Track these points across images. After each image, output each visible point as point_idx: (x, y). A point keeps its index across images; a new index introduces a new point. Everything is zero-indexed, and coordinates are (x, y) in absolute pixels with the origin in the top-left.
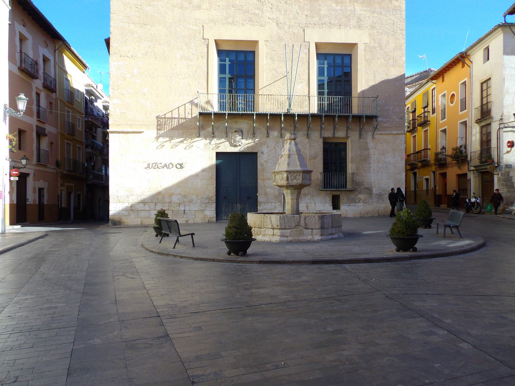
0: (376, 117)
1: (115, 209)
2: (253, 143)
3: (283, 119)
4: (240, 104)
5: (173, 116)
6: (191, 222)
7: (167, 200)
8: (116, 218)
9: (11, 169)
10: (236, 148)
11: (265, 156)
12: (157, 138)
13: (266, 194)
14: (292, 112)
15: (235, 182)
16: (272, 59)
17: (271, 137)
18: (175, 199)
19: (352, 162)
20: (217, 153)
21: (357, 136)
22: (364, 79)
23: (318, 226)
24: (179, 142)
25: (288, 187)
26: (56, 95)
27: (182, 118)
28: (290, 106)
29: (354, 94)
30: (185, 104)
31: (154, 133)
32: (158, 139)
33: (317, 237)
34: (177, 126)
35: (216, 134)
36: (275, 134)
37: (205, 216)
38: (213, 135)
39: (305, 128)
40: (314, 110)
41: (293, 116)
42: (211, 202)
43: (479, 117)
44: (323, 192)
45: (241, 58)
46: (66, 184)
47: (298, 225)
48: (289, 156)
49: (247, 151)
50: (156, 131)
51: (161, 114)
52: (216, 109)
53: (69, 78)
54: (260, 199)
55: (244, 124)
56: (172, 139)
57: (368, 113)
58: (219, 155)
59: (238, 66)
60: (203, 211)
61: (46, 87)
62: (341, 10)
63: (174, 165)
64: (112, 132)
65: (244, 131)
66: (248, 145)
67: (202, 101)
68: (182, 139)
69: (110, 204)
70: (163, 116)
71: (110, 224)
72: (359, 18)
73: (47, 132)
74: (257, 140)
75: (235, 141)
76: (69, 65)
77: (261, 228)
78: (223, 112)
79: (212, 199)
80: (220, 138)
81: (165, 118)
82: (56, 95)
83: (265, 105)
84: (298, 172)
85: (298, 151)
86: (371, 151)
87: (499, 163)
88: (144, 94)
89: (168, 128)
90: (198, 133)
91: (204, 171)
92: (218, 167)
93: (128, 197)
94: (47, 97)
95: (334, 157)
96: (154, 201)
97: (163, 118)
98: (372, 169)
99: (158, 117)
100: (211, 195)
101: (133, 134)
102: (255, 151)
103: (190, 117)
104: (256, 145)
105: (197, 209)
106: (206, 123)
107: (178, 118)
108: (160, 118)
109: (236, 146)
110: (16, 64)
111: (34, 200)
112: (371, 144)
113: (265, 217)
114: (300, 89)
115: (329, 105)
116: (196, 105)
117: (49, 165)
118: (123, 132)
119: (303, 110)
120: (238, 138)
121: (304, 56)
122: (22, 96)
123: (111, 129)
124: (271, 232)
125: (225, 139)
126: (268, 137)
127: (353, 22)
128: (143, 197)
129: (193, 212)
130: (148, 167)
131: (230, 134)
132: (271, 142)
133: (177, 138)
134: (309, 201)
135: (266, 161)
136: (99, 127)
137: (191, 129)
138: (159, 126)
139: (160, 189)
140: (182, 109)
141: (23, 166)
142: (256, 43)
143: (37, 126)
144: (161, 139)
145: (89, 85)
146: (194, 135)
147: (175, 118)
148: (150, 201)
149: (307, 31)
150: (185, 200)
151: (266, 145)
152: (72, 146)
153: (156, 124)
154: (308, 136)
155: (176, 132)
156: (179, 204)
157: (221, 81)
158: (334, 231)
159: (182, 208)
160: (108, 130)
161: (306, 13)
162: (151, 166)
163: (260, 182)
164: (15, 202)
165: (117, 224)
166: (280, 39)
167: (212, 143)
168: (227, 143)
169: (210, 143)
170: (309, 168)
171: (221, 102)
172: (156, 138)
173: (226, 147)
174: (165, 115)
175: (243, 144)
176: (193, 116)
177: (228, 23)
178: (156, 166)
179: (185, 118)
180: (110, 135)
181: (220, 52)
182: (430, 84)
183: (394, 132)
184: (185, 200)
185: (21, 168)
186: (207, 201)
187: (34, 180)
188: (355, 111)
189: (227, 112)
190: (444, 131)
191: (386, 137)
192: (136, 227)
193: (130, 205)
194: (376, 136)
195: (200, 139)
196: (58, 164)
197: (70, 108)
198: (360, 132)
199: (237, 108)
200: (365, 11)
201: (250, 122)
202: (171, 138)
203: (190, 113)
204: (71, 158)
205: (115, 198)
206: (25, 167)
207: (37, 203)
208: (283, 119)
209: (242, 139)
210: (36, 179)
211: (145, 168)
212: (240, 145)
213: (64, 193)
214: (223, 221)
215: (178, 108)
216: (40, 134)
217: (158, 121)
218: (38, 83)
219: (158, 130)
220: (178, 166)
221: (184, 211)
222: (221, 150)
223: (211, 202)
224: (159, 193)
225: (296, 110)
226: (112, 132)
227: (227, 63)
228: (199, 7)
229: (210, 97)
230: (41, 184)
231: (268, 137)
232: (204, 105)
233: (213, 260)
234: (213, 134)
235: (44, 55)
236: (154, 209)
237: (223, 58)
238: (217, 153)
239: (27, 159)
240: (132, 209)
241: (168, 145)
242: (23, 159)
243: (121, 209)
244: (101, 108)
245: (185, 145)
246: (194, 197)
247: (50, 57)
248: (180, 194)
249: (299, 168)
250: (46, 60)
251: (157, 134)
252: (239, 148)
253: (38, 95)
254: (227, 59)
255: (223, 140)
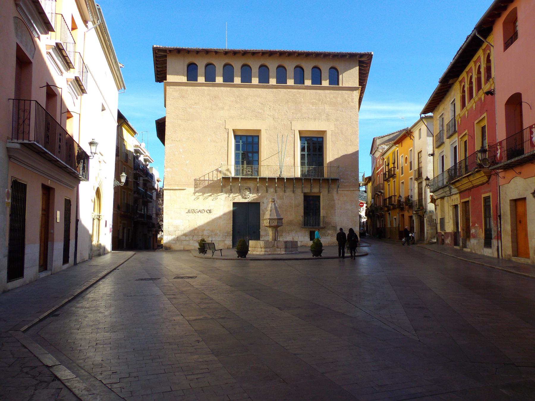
0: (338, 179)
7: (200, 234)
8: (167, 245)
11: (265, 205)
12: (195, 193)
14: (282, 176)
15: (245, 221)
16: (270, 141)
17: (269, 192)
19: (323, 209)
20: (234, 203)
21: (327, 192)
22: (331, 154)
23: (284, 247)
25: (270, 227)
29: (325, 165)
31: (192, 190)
33: (284, 253)
35: (233, 190)
36: (272, 190)
37: (225, 244)
38: (231, 191)
40: (298, 175)
41: (283, 179)
43: (417, 177)
44: (304, 229)
45: (250, 140)
46: (123, 222)
47: (274, 246)
48: (271, 211)
51: (197, 178)
52: (233, 175)
55: (251, 184)
57: (333, 177)
58: (235, 204)
59: (248, 146)
60: (224, 241)
62: (316, 109)
67: (223, 169)
72: (328, 115)
75: (245, 195)
80: (235, 193)
81: (200, 180)
83: (265, 172)
84: (274, 219)
85: (276, 208)
86: (336, 202)
87: (426, 209)
89: (202, 186)
91: (224, 214)
92: (234, 212)
95: (311, 206)
98: (337, 214)
104: (259, 197)
106: (226, 184)
107: (209, 180)
109: (246, 198)
112: (336, 197)
114: (288, 160)
115: (308, 171)
116: (220, 172)
118: (173, 190)
121: (291, 138)
122: (124, 174)
124: (260, 250)
126: (267, 192)
127: (324, 117)
128: (185, 232)
130: (189, 212)
131: (242, 190)
136: (142, 176)
138: (196, 186)
139: (196, 226)
140: (211, 174)
142: (259, 131)
144: (197, 194)
145: (137, 146)
149: (293, 123)
154: (294, 192)
157: (237, 155)
158: (293, 249)
161: (292, 111)
165: (167, 249)
166: (275, 128)
168: (240, 197)
170: (282, 217)
173: (239, 199)
175: (250, 197)
177: (241, 119)
178: (193, 211)
181: (236, 136)
182: (394, 147)
183: (351, 189)
186: (226, 234)
188: (326, 176)
190: (403, 183)
191: (345, 192)
192: (180, 251)
194: (339, 192)
198: (329, 189)
200: (332, 109)
202: (204, 193)
213: (121, 228)
220: (208, 212)
222: (236, 201)
224: (195, 229)
225: (286, 175)
227: (241, 143)
228: (223, 109)
229: (229, 167)
231: (267, 192)
232: (225, 172)
233: (231, 259)
237: (238, 140)
238: (234, 203)
240: (177, 239)
244: (143, 161)
245: (213, 198)
246: (218, 232)
249: (276, 217)
254: (241, 141)
255: (237, 194)
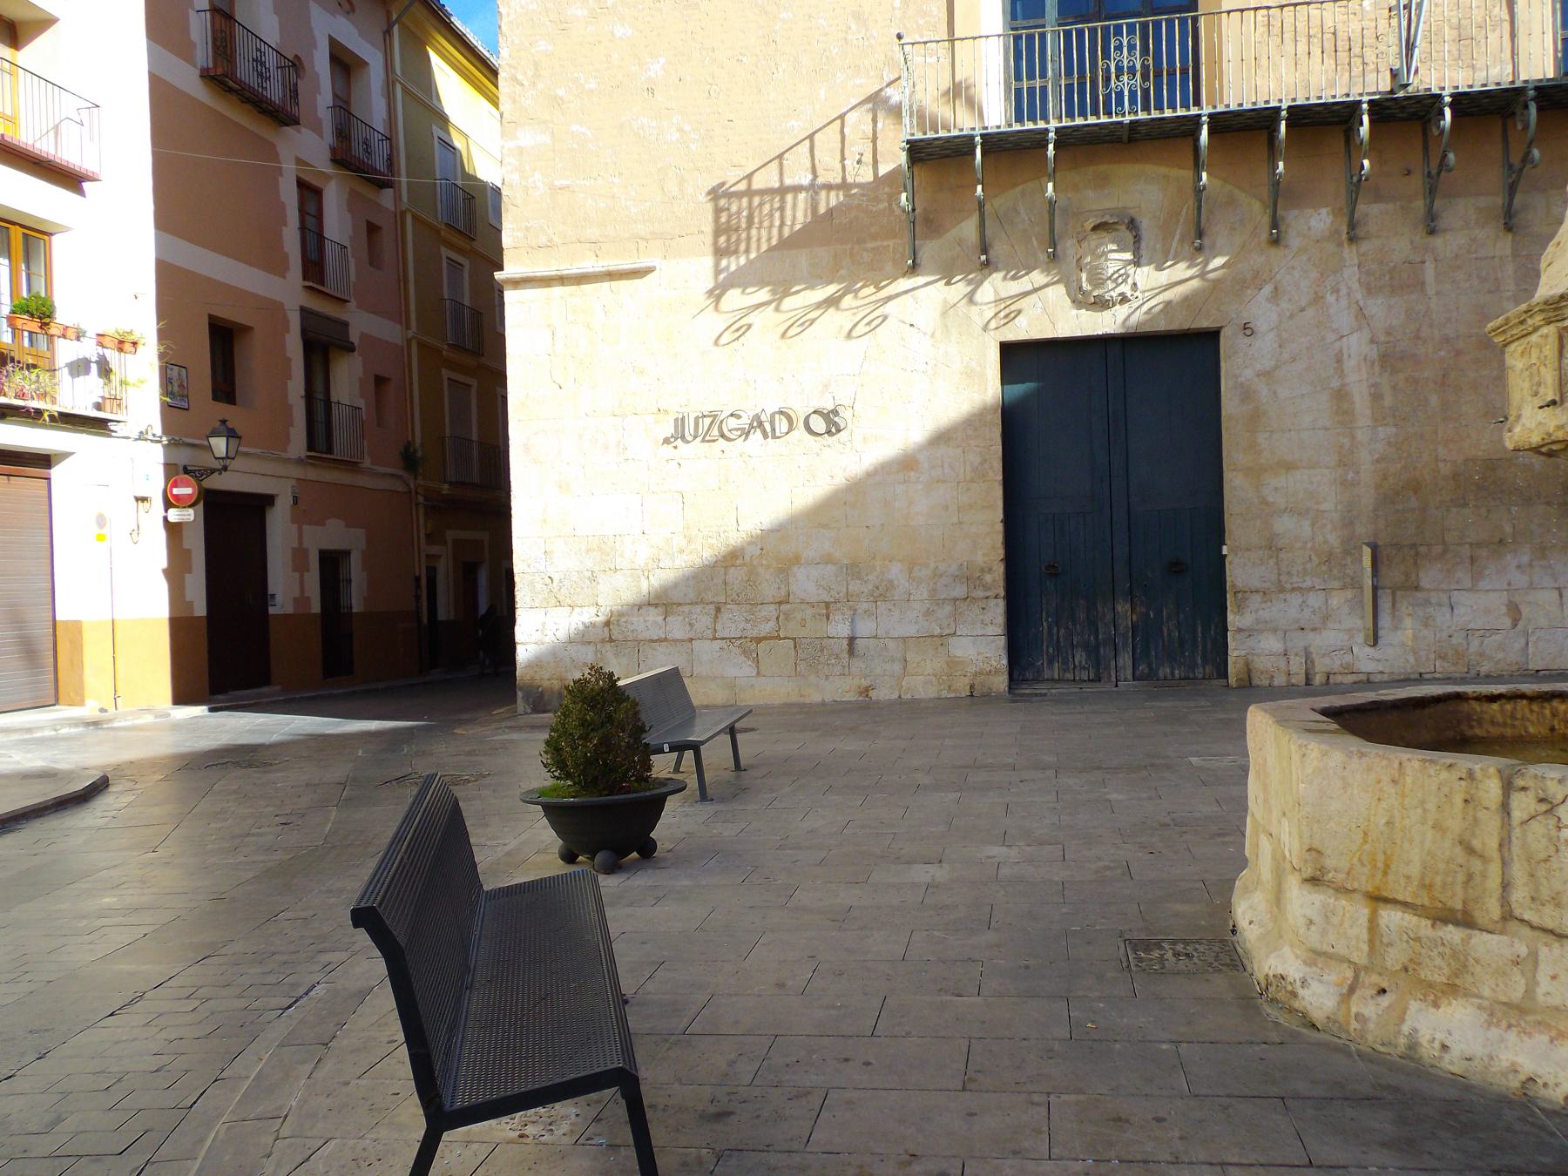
1: (537, 636)
2: (1195, 283)
3: (1365, 130)
4: (1119, 70)
5: (788, 182)
6: (883, 694)
7: (769, 589)
9: (167, 478)
10: (1107, 314)
12: (716, 294)
13: (1273, 547)
17: (1294, 241)
18: (806, 584)
24: (819, 305)
26: (397, 198)
27: (829, 187)
28: (1410, 47)
30: (842, 117)
31: (700, 269)
32: (718, 298)
34: (805, 227)
35: (999, 249)
37: (953, 664)
38: (984, 260)
39: (1493, 177)
41: (1431, 103)
42: (980, 593)
46: (450, 535)
49: (1162, 326)
50: (709, 261)
51: (732, 176)
53: (458, 142)
54: (1239, 571)
55: (1145, 188)
56: (787, 293)
58: (1013, 354)
61: (343, 158)
63: (800, 412)
64: (519, 283)
65: (1145, 224)
66: (1167, 296)
68: (831, 289)
69: (518, 612)
70: (742, 186)
71: (521, 705)
73: (354, 337)
74: (1218, 261)
75: (1098, 281)
76: (452, 88)
77: (1466, 921)
78: (1029, 126)
79: (988, 578)
80: (1019, 267)
82: (397, 198)
88: (651, 91)
89: (764, 238)
90: (908, 251)
91: (941, 438)
92: (1012, 419)
93: (593, 578)
94: (354, 202)
96: (709, 597)
97: (739, 195)
99: (715, 194)
100: (980, 559)
101: (606, 285)
102: (1205, 323)
103: (866, 176)
104: (1214, 290)
105: (911, 630)
106: (952, 193)
107: (813, 188)
108: (729, 195)
109: (1101, 304)
110: (188, 57)
111: (302, 600)
113: (1522, 805)
116: (896, 112)
117: (367, 463)
118: (562, 280)
119: (1489, 70)
120: (1116, 259)
123: (512, 268)
125: (1047, 271)
129: (891, 645)
130: (679, 434)
131: (1069, 246)
132: (1294, 268)
133: (811, 287)
134: (1520, 580)
135: (1266, 374)
137: (874, 238)
140: (827, 142)
141: (217, 465)
143: (303, 310)
144: (735, 299)
146: (889, 267)
147: (797, 189)
148: (692, 596)
150: (855, 587)
151: (1267, 290)
152: (474, 392)
153: (708, 228)
155: (803, 258)
156: (827, 609)
159: (840, 628)
160: (498, 275)
162: (689, 430)
163: (1235, 483)
164: (201, 610)
167: (978, 297)
168: (1057, 294)
169: (970, 298)
171: (1019, 92)
172: (710, 293)
173: (1053, 314)
174: (749, 177)
175: (1141, 291)
176: (884, 169)
178: (709, 428)
179: (844, 186)
180: (510, 296)
184: (855, 587)
185: (213, 471)
186: (960, 591)
187: (294, 519)
189: (1054, 124)
193: (602, 618)
195: (920, 280)
196: (410, 460)
197: (461, 251)
199: (1108, 97)
201: (1175, 172)
202: (782, 290)
203: (868, 158)
204: (475, 437)
205: (538, 586)
206: (225, 468)
207: (316, 608)
208: (1365, 130)
209: (1137, 263)
210: (304, 511)
211: (666, 441)
212: (1124, 299)
213: (444, 569)
214: (1042, 688)
215: (811, 137)
216: (323, 344)
217: (718, 211)
218: (307, 147)
219: (719, 253)
220: (818, 424)
221: (852, 640)
222: (1027, 328)
223: (980, 593)
224: (732, 558)
225: (1442, 75)
226: (519, 283)
230: (332, 534)
231: (1275, 241)
234: (985, 251)
235: (333, 43)
236: (709, 633)
239: (231, 434)
241: (767, 322)
242: (215, 434)
243: (562, 635)
246: (896, 571)
247: (372, 56)
248: (828, 560)
250: (344, 64)
251: (717, 272)
252: (1121, 311)
253: (309, 192)
255: (1038, 277)
